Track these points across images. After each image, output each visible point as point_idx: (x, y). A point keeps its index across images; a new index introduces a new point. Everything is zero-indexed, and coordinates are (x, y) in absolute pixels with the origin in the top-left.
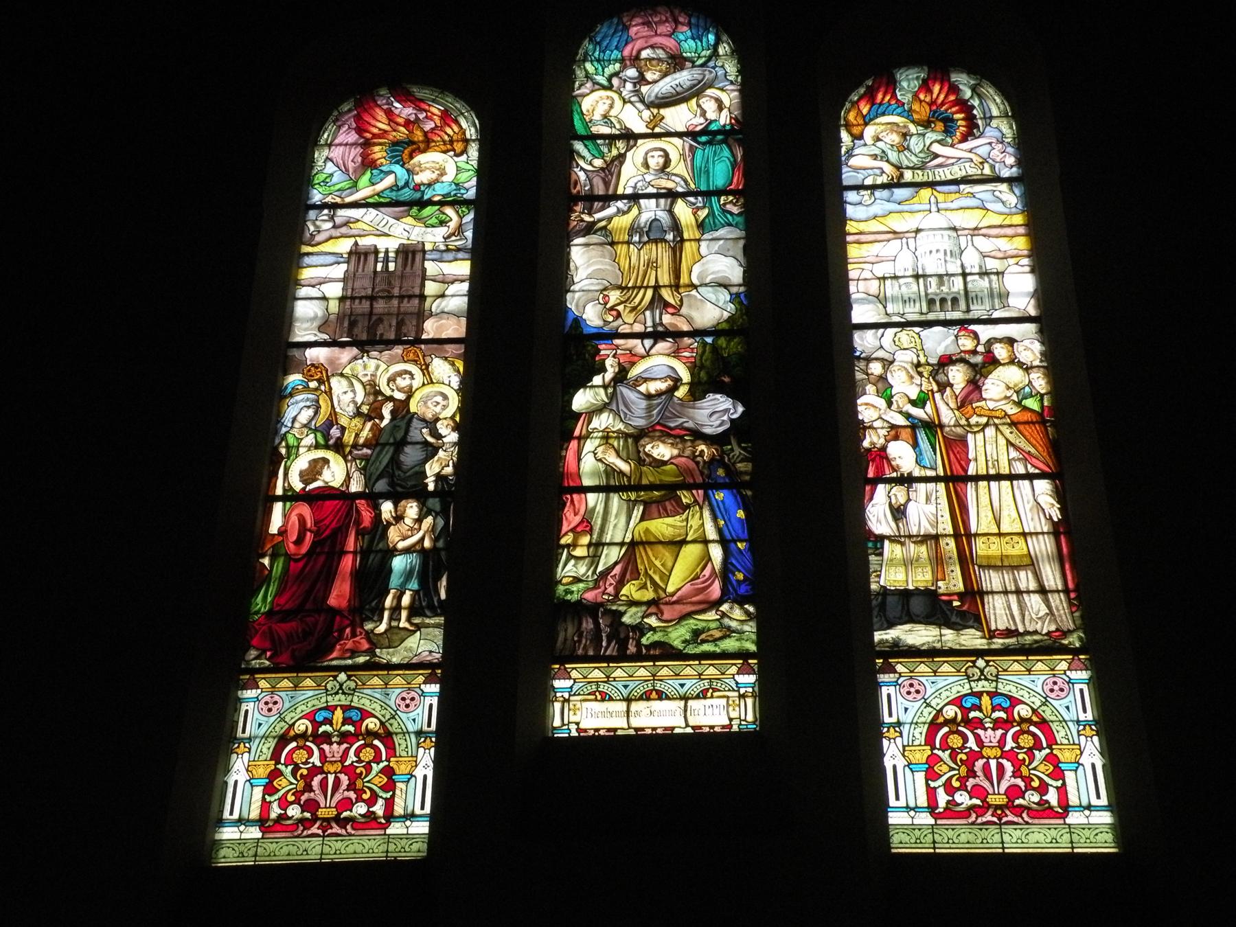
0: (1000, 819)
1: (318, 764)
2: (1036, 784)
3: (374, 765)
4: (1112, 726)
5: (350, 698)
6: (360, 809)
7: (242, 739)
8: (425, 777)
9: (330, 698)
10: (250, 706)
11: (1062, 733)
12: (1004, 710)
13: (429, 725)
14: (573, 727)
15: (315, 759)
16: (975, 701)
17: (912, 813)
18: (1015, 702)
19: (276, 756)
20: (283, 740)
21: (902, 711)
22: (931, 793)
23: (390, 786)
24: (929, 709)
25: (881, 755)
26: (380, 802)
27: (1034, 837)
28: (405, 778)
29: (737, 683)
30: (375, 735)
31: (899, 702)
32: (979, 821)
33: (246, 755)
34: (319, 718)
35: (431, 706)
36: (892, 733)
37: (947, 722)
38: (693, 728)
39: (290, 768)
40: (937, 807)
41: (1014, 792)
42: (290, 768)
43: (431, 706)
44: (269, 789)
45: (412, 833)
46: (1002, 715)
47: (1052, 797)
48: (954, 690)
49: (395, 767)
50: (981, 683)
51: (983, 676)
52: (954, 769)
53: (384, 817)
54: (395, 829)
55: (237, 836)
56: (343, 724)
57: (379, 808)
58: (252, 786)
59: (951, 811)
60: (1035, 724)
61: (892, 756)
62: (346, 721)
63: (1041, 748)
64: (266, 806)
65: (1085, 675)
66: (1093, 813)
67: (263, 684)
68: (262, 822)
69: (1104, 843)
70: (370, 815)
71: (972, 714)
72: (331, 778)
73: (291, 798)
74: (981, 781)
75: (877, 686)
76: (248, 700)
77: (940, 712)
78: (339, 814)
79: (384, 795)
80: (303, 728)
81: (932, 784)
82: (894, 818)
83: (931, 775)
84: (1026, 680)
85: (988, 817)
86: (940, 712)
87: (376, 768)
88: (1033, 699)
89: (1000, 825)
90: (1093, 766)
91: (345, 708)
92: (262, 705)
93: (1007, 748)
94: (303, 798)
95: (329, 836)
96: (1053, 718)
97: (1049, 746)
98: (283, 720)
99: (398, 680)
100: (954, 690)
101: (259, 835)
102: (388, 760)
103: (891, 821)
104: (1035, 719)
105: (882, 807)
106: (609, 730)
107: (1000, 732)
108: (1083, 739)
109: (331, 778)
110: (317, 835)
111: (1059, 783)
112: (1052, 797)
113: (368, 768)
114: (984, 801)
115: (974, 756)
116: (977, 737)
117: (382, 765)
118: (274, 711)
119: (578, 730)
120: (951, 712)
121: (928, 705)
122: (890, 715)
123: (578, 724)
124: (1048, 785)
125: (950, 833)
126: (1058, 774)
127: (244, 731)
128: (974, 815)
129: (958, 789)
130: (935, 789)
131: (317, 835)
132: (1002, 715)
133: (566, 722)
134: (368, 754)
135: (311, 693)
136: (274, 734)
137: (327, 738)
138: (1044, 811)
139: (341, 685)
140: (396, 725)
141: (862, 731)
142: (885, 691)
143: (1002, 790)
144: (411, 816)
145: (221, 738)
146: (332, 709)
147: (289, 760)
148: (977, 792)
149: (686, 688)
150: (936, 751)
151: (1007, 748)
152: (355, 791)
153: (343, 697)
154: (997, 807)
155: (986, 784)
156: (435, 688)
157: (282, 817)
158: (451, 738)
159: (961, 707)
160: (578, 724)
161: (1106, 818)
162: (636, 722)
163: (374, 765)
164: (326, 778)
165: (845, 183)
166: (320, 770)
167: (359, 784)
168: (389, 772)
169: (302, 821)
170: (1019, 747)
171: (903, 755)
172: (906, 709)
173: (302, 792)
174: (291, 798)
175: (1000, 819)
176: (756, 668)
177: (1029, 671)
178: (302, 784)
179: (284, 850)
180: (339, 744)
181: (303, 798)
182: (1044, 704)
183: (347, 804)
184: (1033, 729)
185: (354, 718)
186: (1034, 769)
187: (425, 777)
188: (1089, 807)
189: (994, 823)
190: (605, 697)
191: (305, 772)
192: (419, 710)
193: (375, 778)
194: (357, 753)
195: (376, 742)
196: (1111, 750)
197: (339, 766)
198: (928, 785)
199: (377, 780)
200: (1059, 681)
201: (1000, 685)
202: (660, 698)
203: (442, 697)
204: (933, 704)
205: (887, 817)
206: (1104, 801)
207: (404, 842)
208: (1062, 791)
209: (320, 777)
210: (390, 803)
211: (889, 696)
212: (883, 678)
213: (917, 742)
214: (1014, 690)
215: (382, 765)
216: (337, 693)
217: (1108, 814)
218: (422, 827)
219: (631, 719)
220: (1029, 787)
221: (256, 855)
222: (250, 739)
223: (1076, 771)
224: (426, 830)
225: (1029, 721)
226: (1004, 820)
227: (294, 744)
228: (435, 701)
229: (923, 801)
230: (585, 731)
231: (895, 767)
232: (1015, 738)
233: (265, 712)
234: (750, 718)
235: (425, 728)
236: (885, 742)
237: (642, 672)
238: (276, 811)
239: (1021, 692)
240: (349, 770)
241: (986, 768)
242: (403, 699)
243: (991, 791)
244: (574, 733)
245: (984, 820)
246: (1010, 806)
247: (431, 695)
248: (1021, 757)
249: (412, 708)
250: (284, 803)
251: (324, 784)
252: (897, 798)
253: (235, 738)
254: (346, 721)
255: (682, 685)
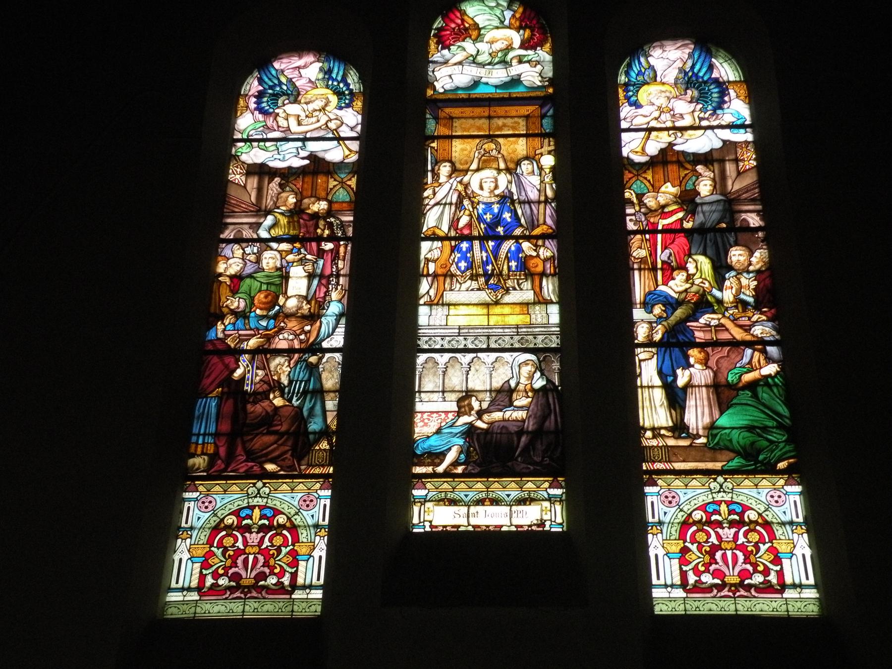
0: (734, 594)
1: (242, 547)
2: (761, 568)
3: (283, 549)
4: (817, 524)
5: (265, 500)
6: (272, 580)
7: (186, 530)
8: (320, 557)
9: (250, 500)
10: (655, 499)
11: (780, 532)
12: (737, 514)
13: (324, 520)
14: (427, 524)
15: (240, 544)
16: (716, 507)
17: (669, 589)
18: (746, 508)
19: (210, 542)
20: (216, 529)
21: (662, 514)
22: (684, 575)
23: (295, 564)
24: (682, 513)
25: (646, 547)
26: (287, 575)
27: (265, 608)
28: (306, 557)
29: (549, 494)
30: (283, 527)
31: (660, 508)
32: (719, 595)
33: (188, 540)
34: (243, 514)
35: (325, 506)
36: (655, 530)
37: (695, 523)
38: (474, 526)
39: (221, 550)
40: (688, 585)
41: (744, 574)
42: (221, 550)
43: (325, 506)
44: (205, 565)
45: (310, 601)
46: (267, 522)
47: (773, 578)
48: (700, 499)
49: (298, 550)
50: (256, 500)
51: (258, 494)
52: (700, 558)
53: (779, 585)
54: (789, 594)
55: (181, 598)
56: (260, 519)
57: (286, 580)
58: (193, 563)
59: (698, 588)
60: (288, 530)
61: (656, 546)
62: (731, 512)
63: (764, 544)
64: (202, 577)
65: (798, 489)
66: (313, 591)
67: (201, 488)
68: (199, 589)
69: (813, 610)
70: (279, 583)
71: (714, 518)
72: (251, 557)
73: (221, 571)
74: (721, 566)
75: (644, 495)
76: (189, 500)
77: (690, 515)
78: (742, 581)
79: (290, 570)
80: (230, 521)
81: (685, 568)
82: (656, 593)
83: (683, 562)
84: (754, 492)
85: (725, 592)
86: (690, 515)
87: (284, 550)
88: (759, 506)
89: (735, 598)
90: (804, 556)
91: (261, 508)
92: (200, 504)
93: (739, 542)
94: (231, 572)
95: (249, 598)
96: (301, 524)
97: (771, 541)
98: (216, 515)
99: (301, 486)
100: (700, 499)
101: (198, 598)
102: (293, 544)
103: (654, 595)
104: (760, 521)
105: (649, 586)
106: (453, 527)
107: (734, 530)
108: (795, 536)
109: (251, 557)
110: (240, 598)
111: (778, 568)
112: (773, 578)
113: (279, 551)
114: (723, 581)
115: (714, 548)
116: (717, 534)
117: (289, 549)
118: (210, 508)
119: (431, 526)
120: (698, 515)
121: (681, 510)
122: (653, 517)
123: (431, 522)
124: (285, 571)
125: (697, 604)
126: (777, 561)
127: (186, 523)
128: (228, 593)
129: (704, 572)
130: (686, 571)
131: (240, 598)
132: (736, 517)
133: (422, 520)
134: (278, 541)
135: (236, 496)
136: (208, 526)
137: (248, 529)
138: (767, 588)
139: (259, 490)
140: (299, 520)
141: (634, 527)
142: (649, 500)
143: (736, 573)
144: (311, 587)
145: (168, 529)
146: (252, 508)
147: (220, 545)
148: (717, 574)
149: (469, 498)
150: (213, 549)
151: (739, 542)
152: (268, 566)
153: (260, 500)
154: (732, 585)
155: (724, 569)
156: (328, 493)
157: (215, 586)
158: (341, 531)
159: (705, 512)
160: (431, 522)
161: (812, 594)
162: (473, 521)
163: (283, 549)
164: (247, 558)
165: (358, 142)
166: (243, 552)
167: (272, 562)
168: (294, 554)
169: (229, 588)
170: (749, 542)
171: (189, 551)
172: (665, 513)
173: (230, 568)
174: (221, 571)
175: (734, 594)
176: (563, 484)
177: (756, 485)
178: (229, 561)
179: (216, 609)
180: (258, 533)
181: (231, 572)
182: (297, 514)
183: (262, 576)
184: (758, 528)
185: (269, 515)
186: (760, 557)
187: (320, 557)
188: (801, 586)
189: (730, 597)
190: (453, 502)
191: (708, 549)
192: (317, 509)
193: (764, 557)
194: (271, 540)
195: (285, 532)
196: (816, 543)
197: (256, 550)
198: (681, 569)
199: (285, 560)
200: (204, 499)
201: (734, 496)
202: (492, 505)
203: (332, 498)
204: (685, 509)
205: (651, 593)
206: (812, 581)
207: (304, 605)
208: (780, 574)
209: (243, 557)
210: (294, 576)
211: (652, 503)
212: (647, 489)
213: (201, 542)
214: (745, 499)
215: (289, 549)
216: (256, 497)
217: (815, 590)
218: (318, 594)
219: (471, 518)
220: (756, 571)
221: (293, 611)
222: (192, 528)
223: (791, 558)
224: (320, 596)
225: (756, 522)
226: (738, 594)
227: (224, 533)
228: (328, 502)
229: (677, 580)
230: (436, 527)
231: (656, 556)
232: (746, 535)
233: (667, 503)
234: (559, 520)
235: (321, 522)
236: (650, 536)
237: (479, 485)
238: (209, 581)
239: (750, 501)
240: (265, 552)
241: (724, 556)
242: (305, 501)
243: (727, 574)
244: (428, 529)
245: (722, 594)
246: (741, 584)
247: (325, 497)
248: (749, 549)
249: (311, 507)
250: (216, 576)
251: (246, 561)
252: (658, 578)
253: (180, 527)
254: (731, 512)
255: (508, 496)
